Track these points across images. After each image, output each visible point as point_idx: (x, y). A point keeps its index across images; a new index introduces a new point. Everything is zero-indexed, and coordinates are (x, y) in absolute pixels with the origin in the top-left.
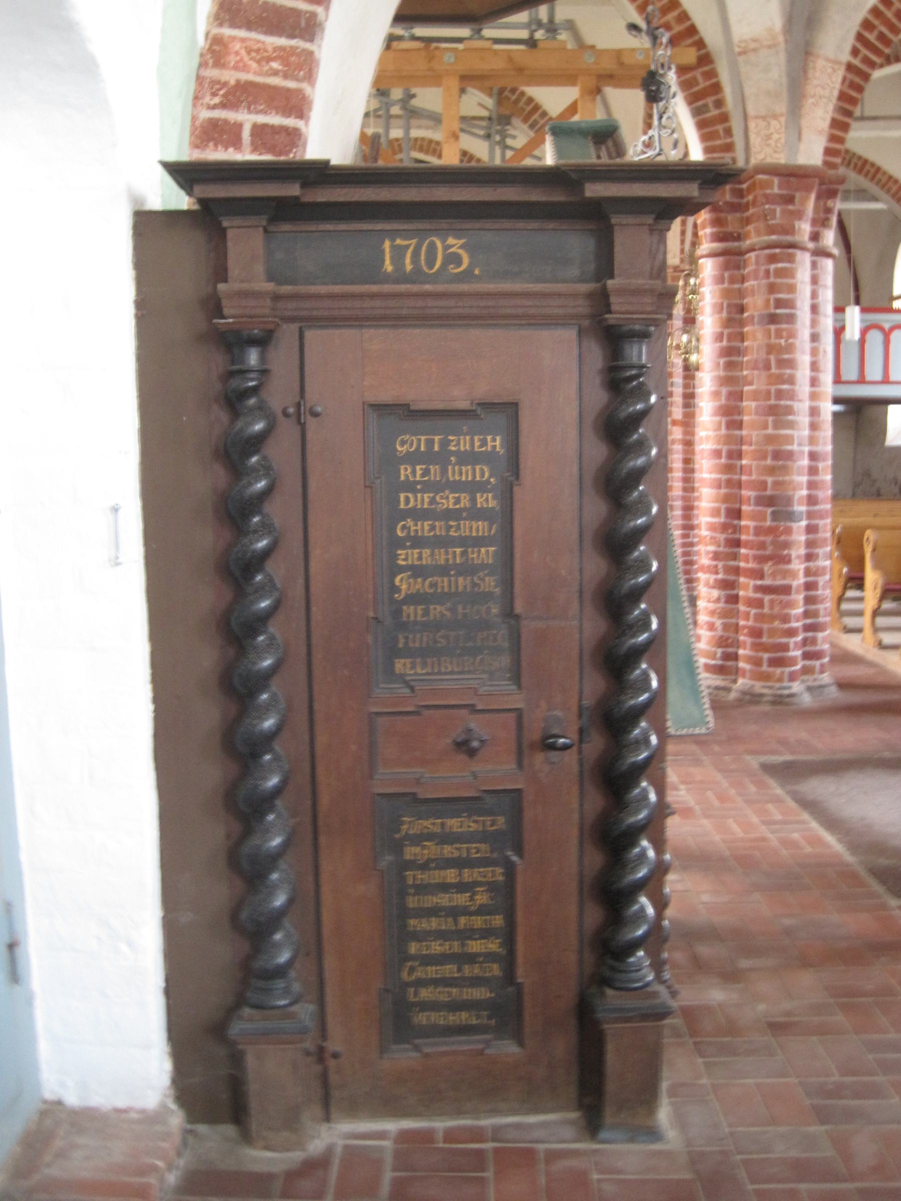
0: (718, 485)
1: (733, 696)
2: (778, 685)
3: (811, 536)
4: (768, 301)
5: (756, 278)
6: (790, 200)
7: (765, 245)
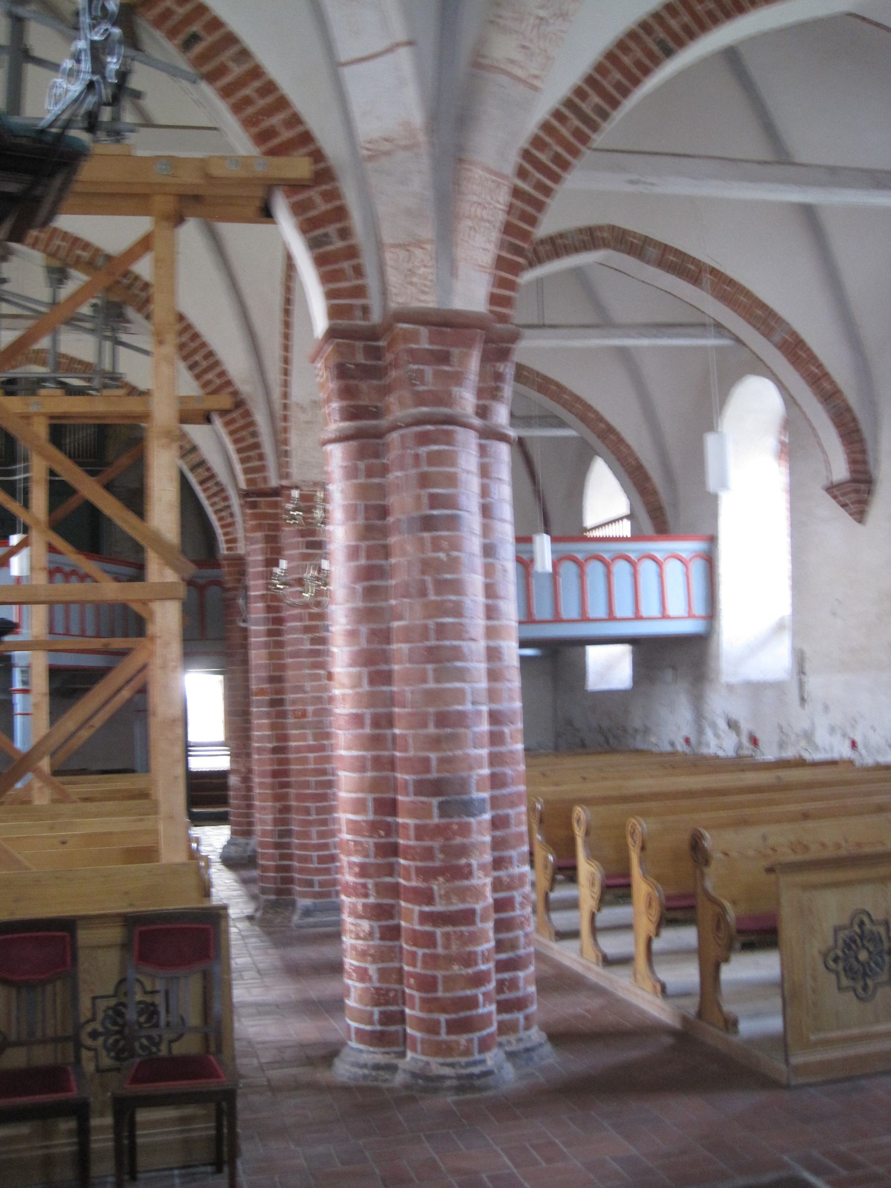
0: (360, 766)
1: (400, 1078)
2: (463, 1060)
3: (498, 833)
4: (418, 498)
5: (402, 468)
6: (443, 358)
7: (409, 420)
